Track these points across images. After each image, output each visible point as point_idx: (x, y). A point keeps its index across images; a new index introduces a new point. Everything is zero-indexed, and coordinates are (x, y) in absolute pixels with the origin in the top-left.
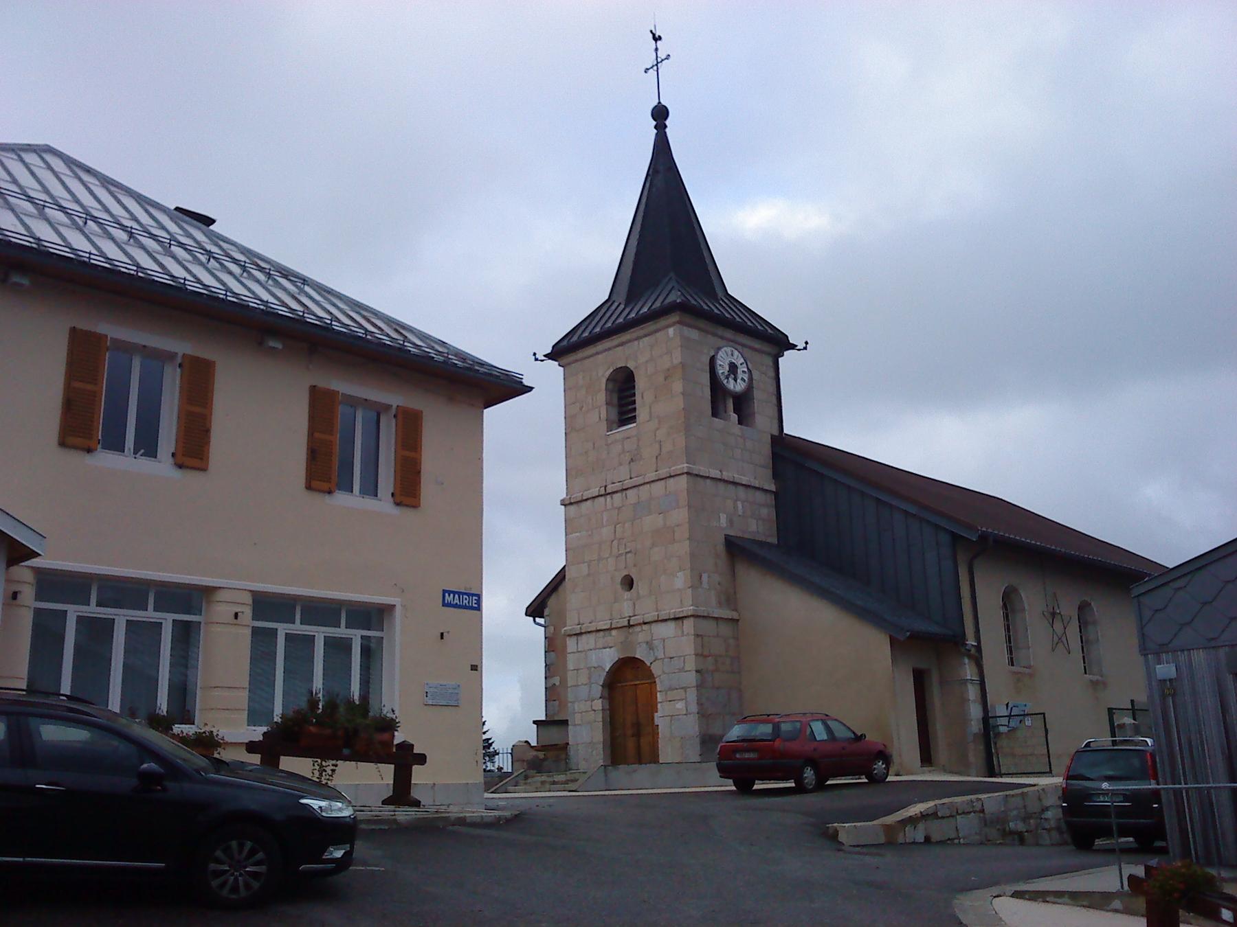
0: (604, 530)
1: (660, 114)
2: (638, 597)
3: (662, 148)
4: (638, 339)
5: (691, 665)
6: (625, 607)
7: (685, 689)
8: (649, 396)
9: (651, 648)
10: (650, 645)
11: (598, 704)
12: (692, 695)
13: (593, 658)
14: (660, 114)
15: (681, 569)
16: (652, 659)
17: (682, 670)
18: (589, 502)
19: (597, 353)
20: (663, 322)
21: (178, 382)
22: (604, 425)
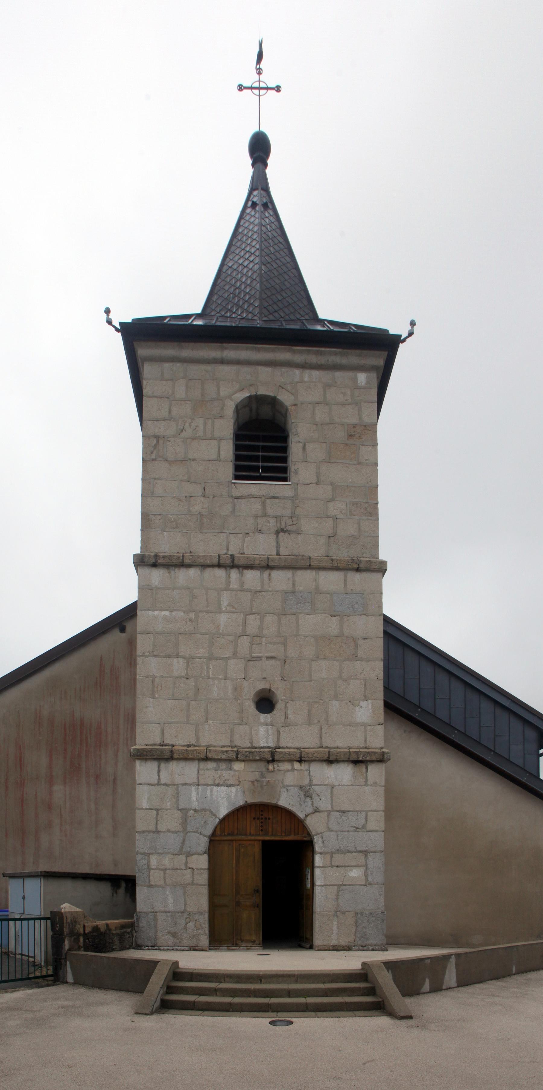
0: (223, 619)
1: (260, 148)
2: (287, 724)
3: (260, 184)
4: (304, 366)
5: (377, 822)
6: (262, 733)
7: (365, 853)
8: (316, 452)
9: (308, 795)
10: (306, 792)
11: (202, 862)
12: (376, 862)
13: (193, 797)
14: (260, 148)
15: (366, 698)
16: (309, 809)
17: (363, 828)
18: (192, 572)
19: (222, 362)
20: (353, 357)
21: (323, 349)
22: (229, 469)
